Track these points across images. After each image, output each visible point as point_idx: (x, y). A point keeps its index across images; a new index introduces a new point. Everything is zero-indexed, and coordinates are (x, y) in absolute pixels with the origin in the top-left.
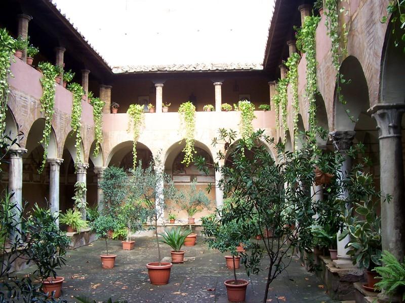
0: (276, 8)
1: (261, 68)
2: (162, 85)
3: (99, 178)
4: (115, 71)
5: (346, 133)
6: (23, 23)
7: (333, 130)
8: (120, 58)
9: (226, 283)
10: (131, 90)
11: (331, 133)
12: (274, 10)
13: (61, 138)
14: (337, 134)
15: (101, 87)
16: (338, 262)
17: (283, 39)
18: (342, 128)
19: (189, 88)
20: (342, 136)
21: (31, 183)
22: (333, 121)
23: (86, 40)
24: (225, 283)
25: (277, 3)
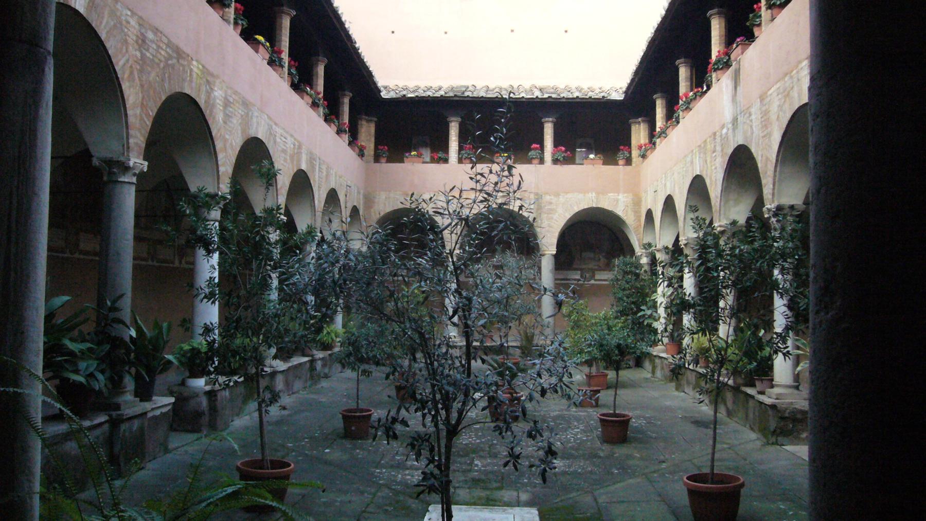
0: (668, 11)
1: (618, 96)
2: (460, 119)
3: (141, 176)
4: (384, 94)
5: (792, 207)
6: (284, 21)
7: (773, 202)
8: (398, 71)
9: (688, 478)
10: (409, 125)
11: (769, 206)
12: (663, 13)
13: (318, 230)
14: (779, 208)
15: (361, 119)
16: (776, 390)
17: (676, 59)
18: (786, 201)
19: (502, 125)
20: (785, 212)
21: (150, 263)
22: (774, 189)
23: (357, 46)
24: (685, 479)
25: (671, 4)
